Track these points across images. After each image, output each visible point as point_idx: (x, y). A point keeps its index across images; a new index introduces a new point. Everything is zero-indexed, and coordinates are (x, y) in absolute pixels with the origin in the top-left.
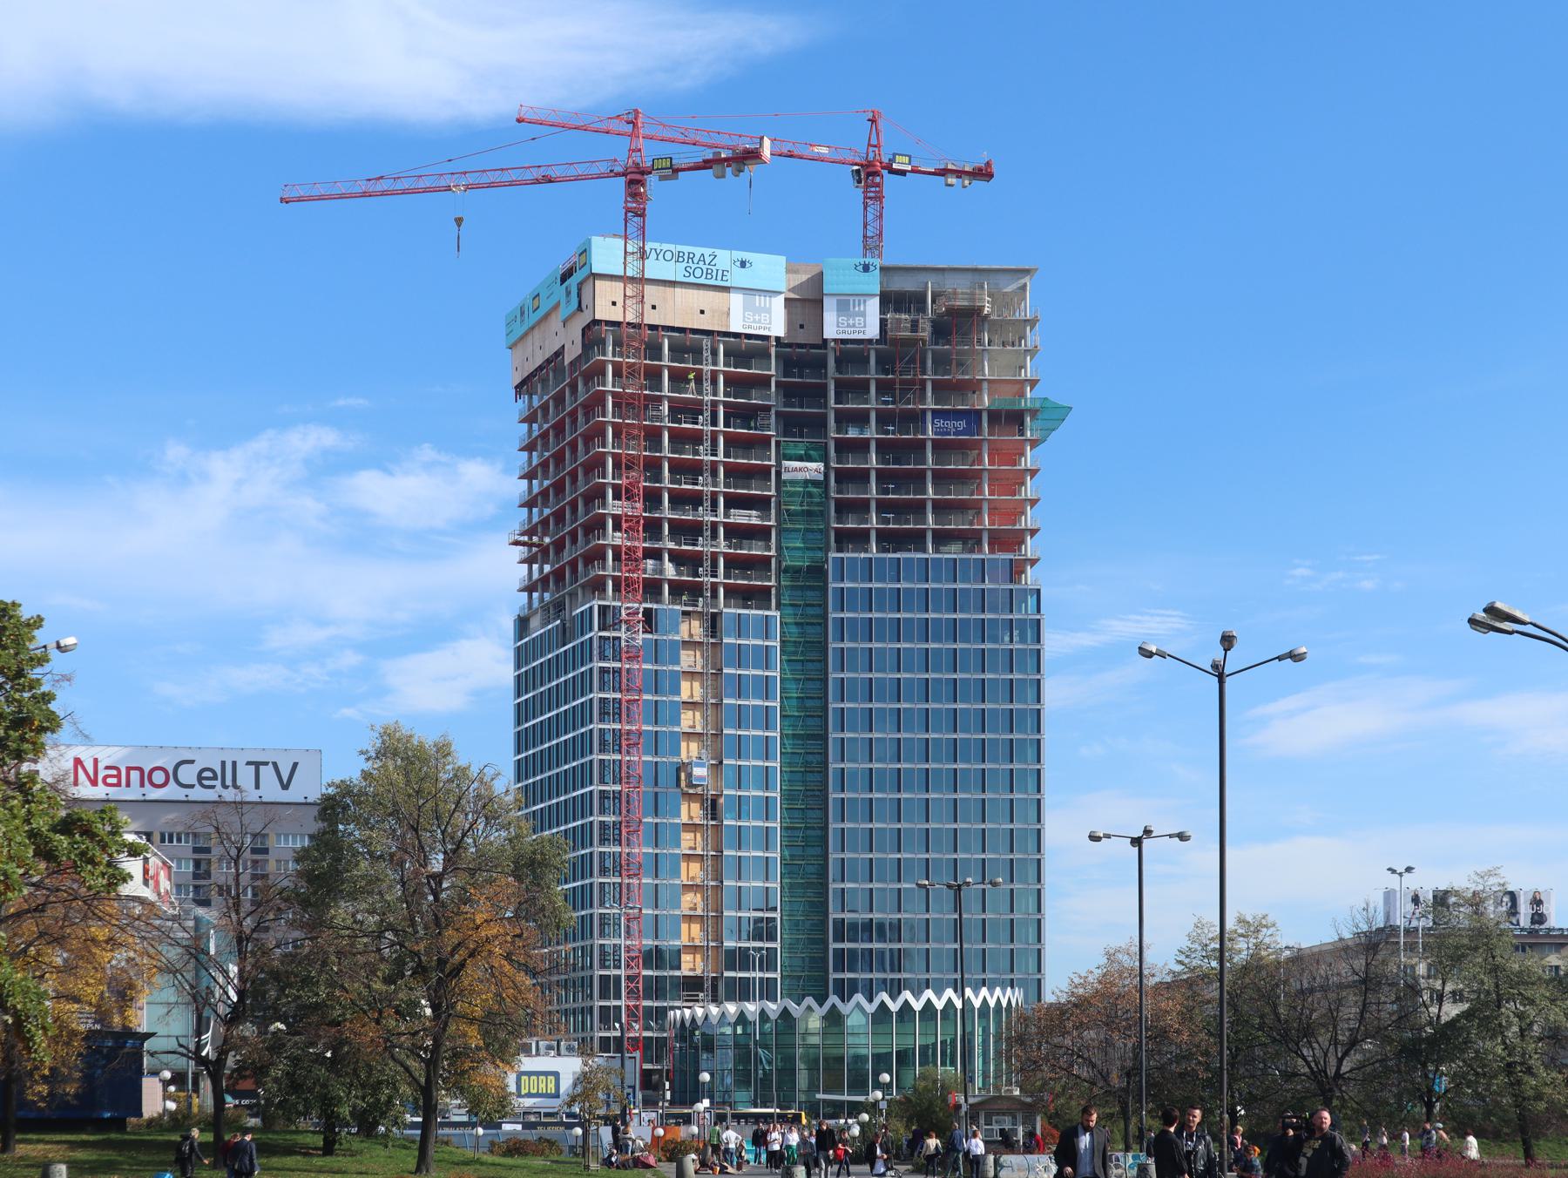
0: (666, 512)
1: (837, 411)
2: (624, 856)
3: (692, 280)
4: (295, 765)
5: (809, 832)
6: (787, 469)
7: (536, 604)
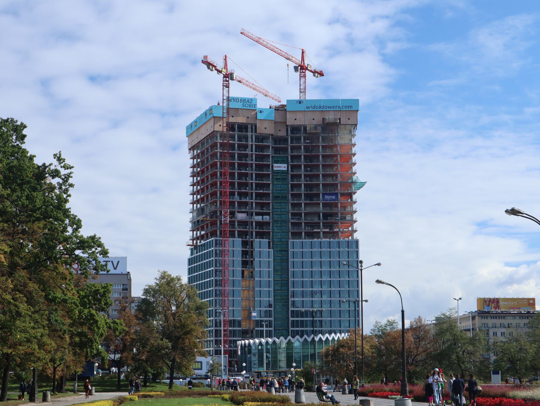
0: (237, 198)
1: (291, 146)
2: (223, 291)
3: (245, 108)
4: (118, 262)
5: (283, 282)
6: (275, 167)
7: (195, 208)
